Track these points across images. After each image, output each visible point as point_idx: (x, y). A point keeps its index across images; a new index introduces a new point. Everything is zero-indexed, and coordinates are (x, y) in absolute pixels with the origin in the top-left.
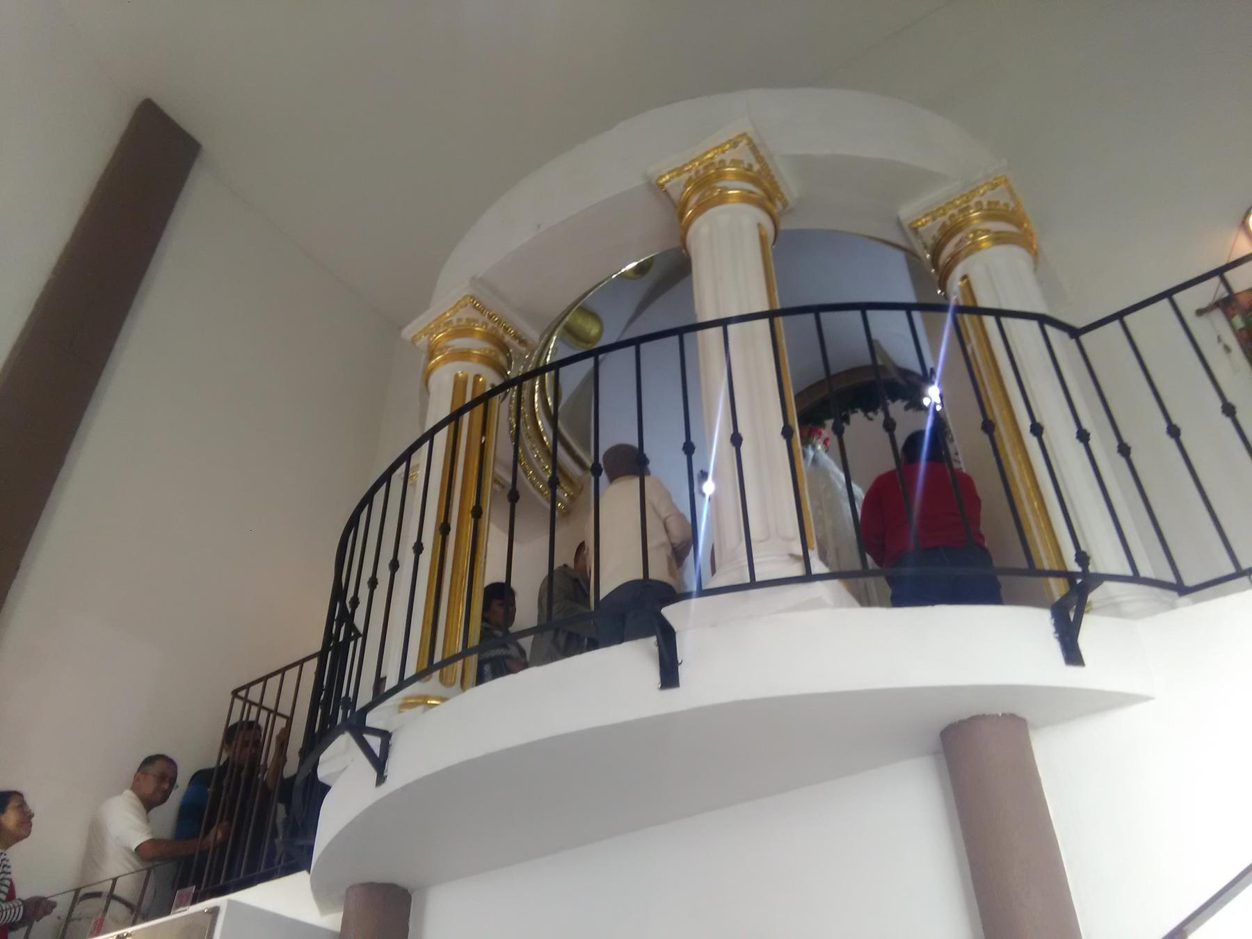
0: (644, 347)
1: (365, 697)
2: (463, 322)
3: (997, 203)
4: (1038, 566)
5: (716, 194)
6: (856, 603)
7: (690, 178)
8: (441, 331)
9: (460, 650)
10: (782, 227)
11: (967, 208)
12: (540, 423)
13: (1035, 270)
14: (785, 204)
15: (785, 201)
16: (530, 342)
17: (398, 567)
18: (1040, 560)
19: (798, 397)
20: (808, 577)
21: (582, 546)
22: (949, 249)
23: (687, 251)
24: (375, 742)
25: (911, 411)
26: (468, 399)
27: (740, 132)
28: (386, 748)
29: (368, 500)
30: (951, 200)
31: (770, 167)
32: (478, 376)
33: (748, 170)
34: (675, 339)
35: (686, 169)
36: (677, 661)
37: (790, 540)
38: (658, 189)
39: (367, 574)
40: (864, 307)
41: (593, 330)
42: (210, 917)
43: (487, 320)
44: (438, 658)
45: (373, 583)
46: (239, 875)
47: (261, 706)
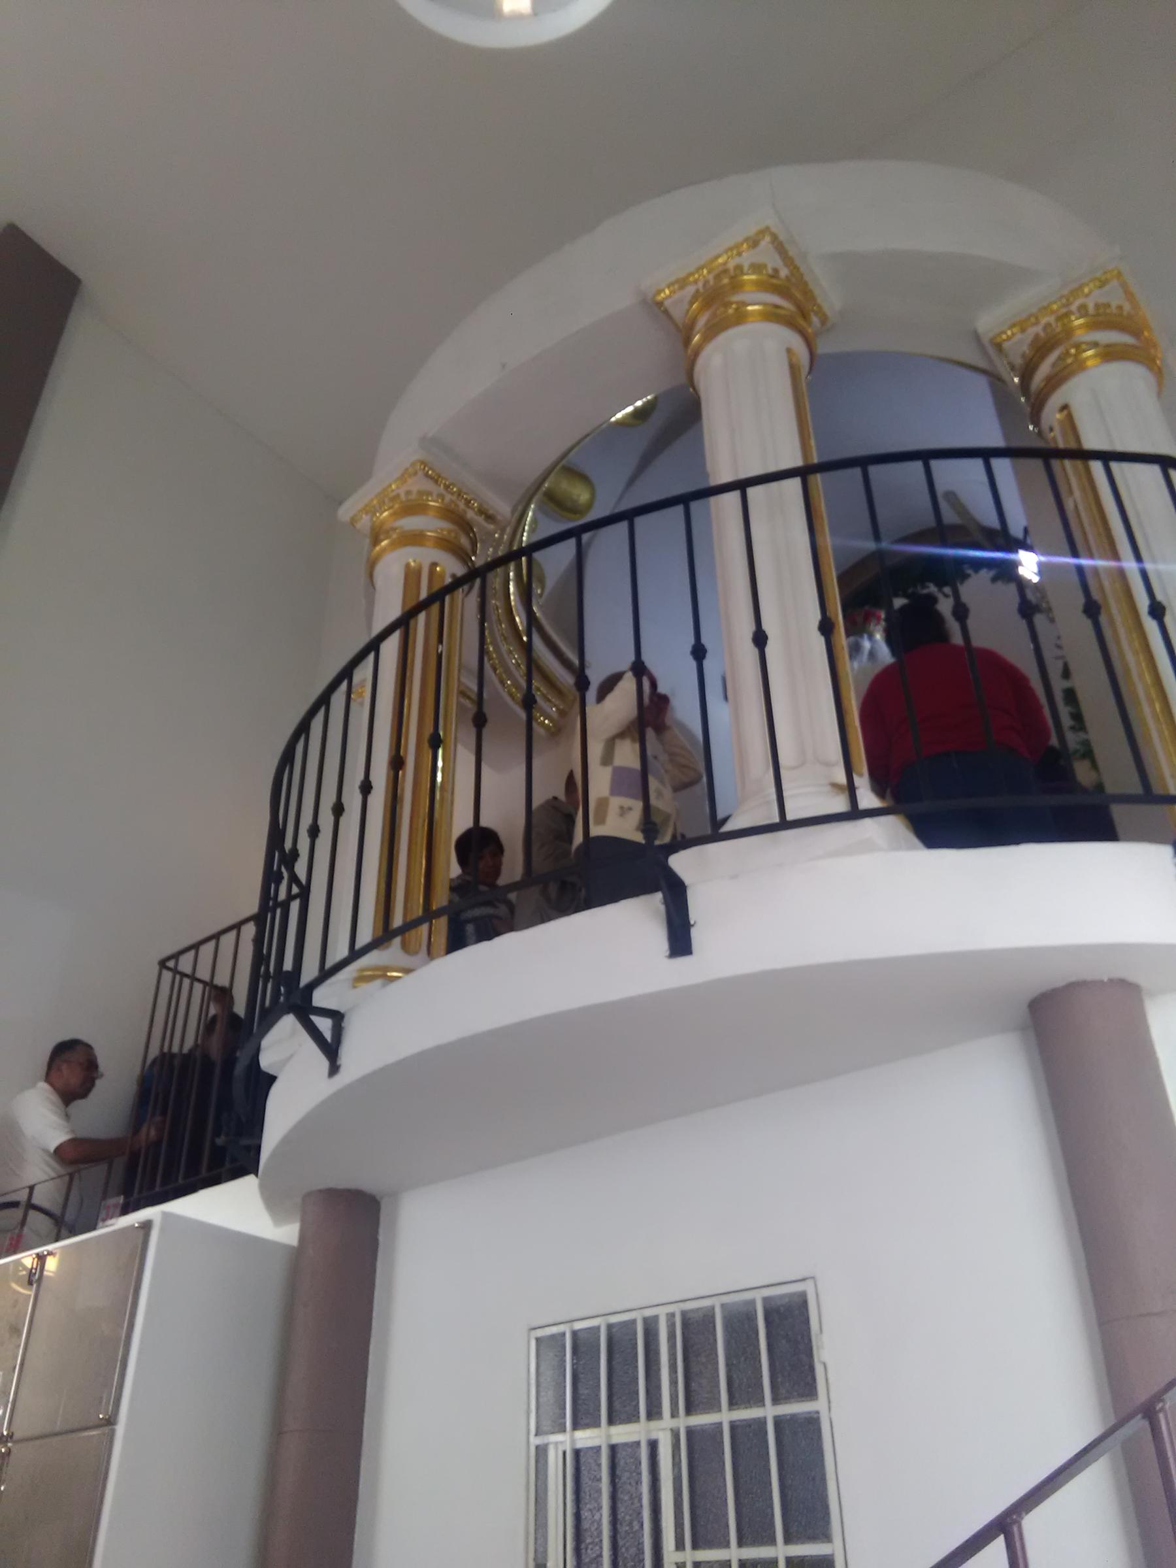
0: (640, 522)
1: (309, 972)
2: (414, 496)
3: (1108, 306)
4: (1157, 790)
5: (731, 311)
6: (915, 841)
7: (697, 291)
8: (386, 508)
9: (420, 912)
10: (823, 348)
11: (1067, 315)
12: (517, 619)
13: (1159, 394)
14: (824, 320)
15: (825, 315)
16: (499, 517)
17: (372, 787)
18: (1162, 778)
19: (843, 579)
20: (855, 813)
21: (571, 777)
22: (1044, 370)
23: (694, 389)
24: (324, 1025)
25: (999, 584)
26: (424, 595)
27: (761, 226)
28: (338, 1031)
29: (303, 729)
30: (1045, 304)
31: (802, 270)
32: (434, 565)
33: (772, 277)
34: (680, 509)
35: (691, 279)
36: (689, 922)
37: (828, 764)
38: (657, 308)
39: (355, 777)
40: (926, 456)
41: (581, 495)
42: (141, 1232)
43: (444, 492)
44: (397, 921)
45: (314, 831)
46: (177, 1180)
47: (194, 978)
